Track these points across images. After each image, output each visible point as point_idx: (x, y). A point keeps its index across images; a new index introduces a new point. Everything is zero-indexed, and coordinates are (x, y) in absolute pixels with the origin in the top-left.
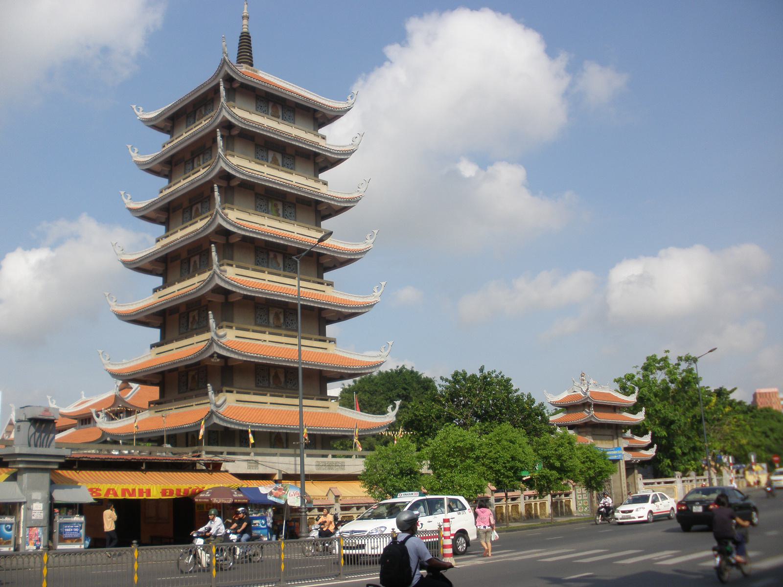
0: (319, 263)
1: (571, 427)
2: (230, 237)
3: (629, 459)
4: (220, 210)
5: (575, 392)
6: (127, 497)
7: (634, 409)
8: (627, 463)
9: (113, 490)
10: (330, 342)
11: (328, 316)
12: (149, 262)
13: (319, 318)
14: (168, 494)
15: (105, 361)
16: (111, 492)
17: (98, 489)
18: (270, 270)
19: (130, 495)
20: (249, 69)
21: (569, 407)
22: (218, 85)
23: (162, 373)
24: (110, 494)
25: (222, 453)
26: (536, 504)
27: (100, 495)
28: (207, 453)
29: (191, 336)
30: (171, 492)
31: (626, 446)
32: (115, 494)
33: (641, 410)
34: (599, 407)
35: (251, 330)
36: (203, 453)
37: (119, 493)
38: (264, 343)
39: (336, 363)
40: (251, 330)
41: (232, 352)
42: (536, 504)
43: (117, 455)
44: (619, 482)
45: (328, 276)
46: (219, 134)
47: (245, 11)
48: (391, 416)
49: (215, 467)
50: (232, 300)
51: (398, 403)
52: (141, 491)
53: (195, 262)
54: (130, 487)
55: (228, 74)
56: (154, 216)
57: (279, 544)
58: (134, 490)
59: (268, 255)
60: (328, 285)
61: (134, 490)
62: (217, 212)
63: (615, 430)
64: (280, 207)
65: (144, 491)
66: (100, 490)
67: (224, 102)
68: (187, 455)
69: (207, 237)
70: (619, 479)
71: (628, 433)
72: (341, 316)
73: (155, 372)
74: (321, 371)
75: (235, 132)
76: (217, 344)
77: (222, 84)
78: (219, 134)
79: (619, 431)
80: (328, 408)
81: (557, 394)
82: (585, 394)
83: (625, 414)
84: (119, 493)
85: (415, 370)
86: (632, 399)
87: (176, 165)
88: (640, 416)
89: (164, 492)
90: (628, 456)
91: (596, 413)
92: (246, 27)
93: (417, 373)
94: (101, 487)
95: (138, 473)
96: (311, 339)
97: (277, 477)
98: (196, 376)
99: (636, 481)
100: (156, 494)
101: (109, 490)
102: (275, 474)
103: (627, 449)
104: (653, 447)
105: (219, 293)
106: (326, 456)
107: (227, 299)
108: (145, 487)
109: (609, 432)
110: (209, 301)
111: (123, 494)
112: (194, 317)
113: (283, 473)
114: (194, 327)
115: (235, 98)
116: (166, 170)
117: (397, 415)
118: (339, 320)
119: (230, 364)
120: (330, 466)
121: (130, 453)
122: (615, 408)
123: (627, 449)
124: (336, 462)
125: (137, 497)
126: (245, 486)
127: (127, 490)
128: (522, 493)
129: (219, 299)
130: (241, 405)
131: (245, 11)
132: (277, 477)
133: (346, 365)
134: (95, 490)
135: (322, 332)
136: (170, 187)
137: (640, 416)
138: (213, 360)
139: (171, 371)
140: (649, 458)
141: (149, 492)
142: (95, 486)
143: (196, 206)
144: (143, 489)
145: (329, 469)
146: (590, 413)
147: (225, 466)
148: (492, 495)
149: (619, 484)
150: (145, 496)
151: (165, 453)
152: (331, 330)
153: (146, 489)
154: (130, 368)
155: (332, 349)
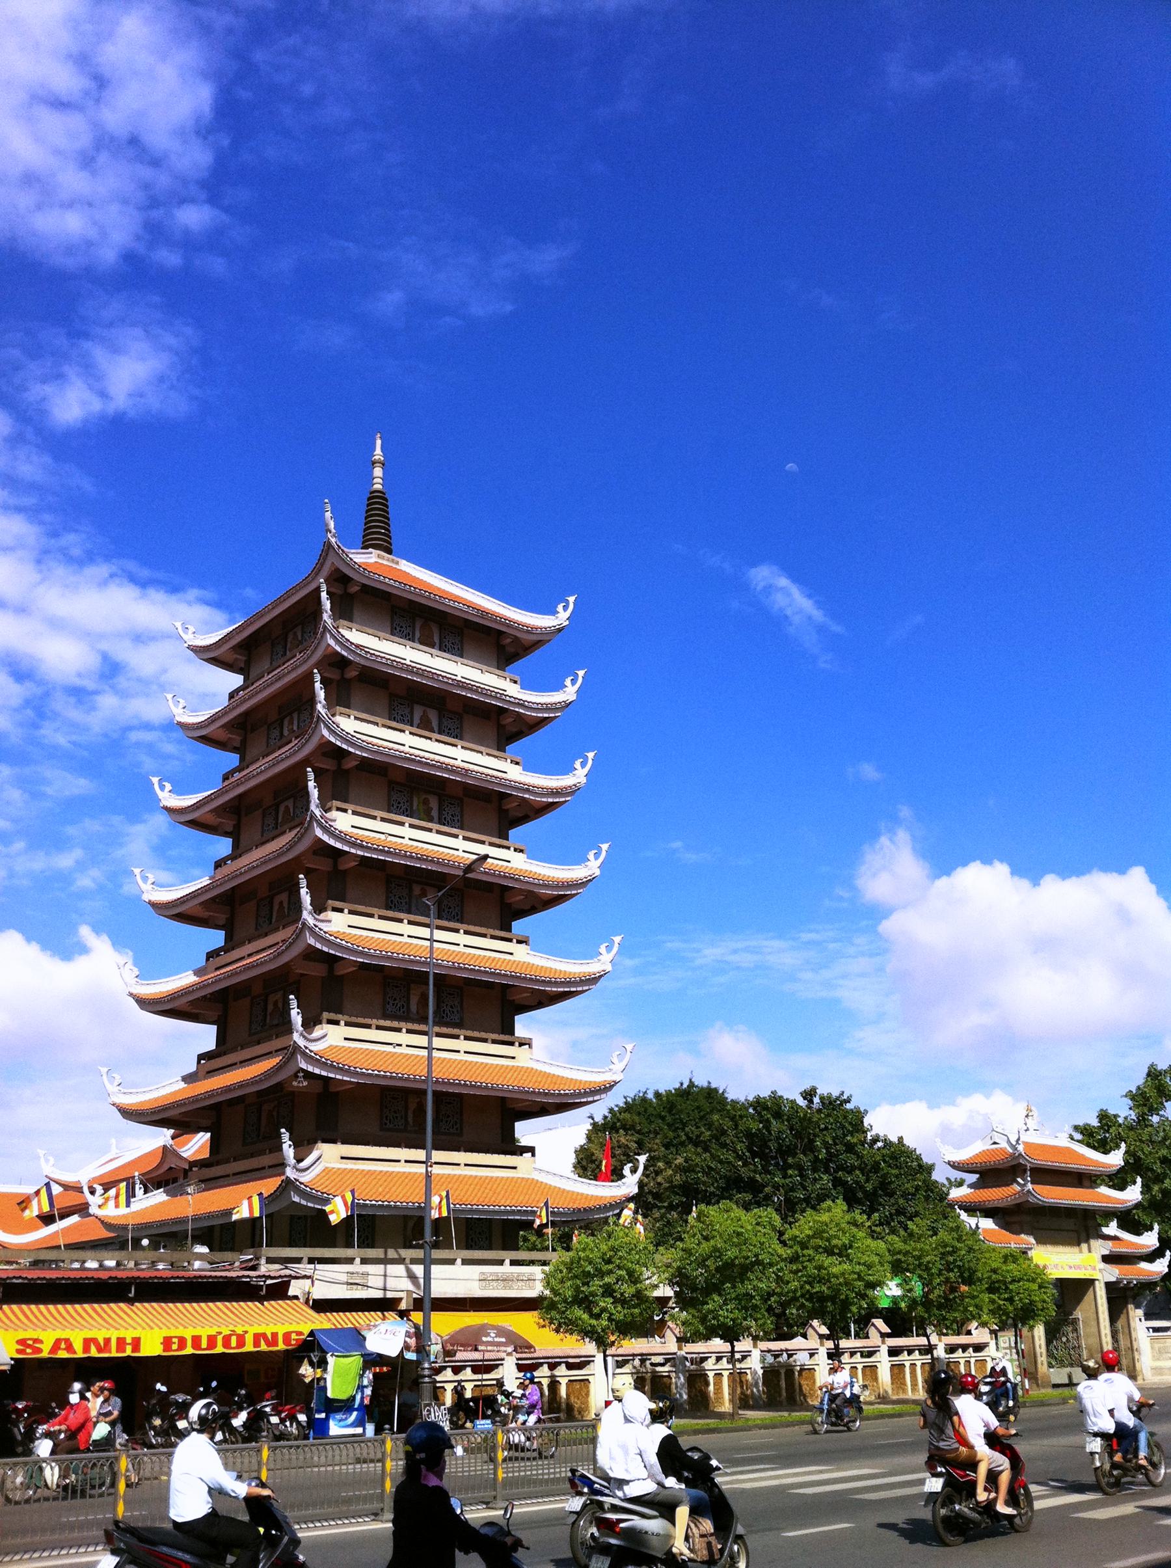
0: (500, 905)
1: (988, 1213)
2: (340, 860)
3: (1114, 1279)
4: (317, 812)
5: (995, 1143)
6: (94, 1353)
7: (1119, 1180)
8: (1108, 1285)
9: (67, 1341)
10: (521, 1045)
11: (517, 998)
12: (200, 904)
13: (493, 1005)
14: (175, 1347)
15: (112, 1088)
16: (63, 1346)
17: (37, 1341)
18: (413, 917)
19: (100, 1350)
20: (383, 558)
21: (994, 1172)
22: (318, 590)
23: (217, 1107)
24: (59, 1348)
25: (298, 1260)
26: (913, 1365)
27: (40, 1351)
28: (270, 1261)
29: (269, 1038)
30: (182, 1342)
31: (1107, 1252)
32: (70, 1347)
33: (1134, 1183)
34: (1044, 1175)
35: (374, 1026)
36: (263, 1261)
37: (78, 1346)
38: (398, 1050)
39: (530, 1084)
40: (374, 1026)
41: (341, 1070)
42: (913, 1365)
43: (96, 1270)
44: (1094, 1323)
45: (519, 926)
46: (318, 678)
47: (378, 451)
48: (629, 1184)
49: (279, 1291)
50: (342, 973)
51: (642, 1159)
52: (121, 1342)
53: (281, 903)
54: (100, 1336)
55: (337, 570)
56: (212, 820)
57: (383, 1442)
58: (107, 1341)
59: (411, 890)
60: (519, 942)
61: (107, 1341)
62: (313, 817)
63: (1079, 1226)
64: (434, 803)
65: (129, 1341)
66: (41, 1342)
67: (329, 621)
68: (233, 1267)
69: (297, 859)
70: (1094, 1318)
71: (1112, 1229)
72: (543, 995)
73: (198, 1106)
74: (503, 1099)
75: (352, 673)
76: (304, 1054)
77: (324, 587)
78: (318, 678)
79: (1090, 1223)
80: (515, 1168)
81: (959, 1146)
82: (1014, 1148)
83: (1104, 1190)
84: (78, 1346)
85: (713, 1086)
86: (1116, 1159)
87: (253, 731)
88: (1133, 1194)
89: (167, 1342)
90: (1112, 1273)
91: (1036, 1187)
92: (380, 481)
93: (716, 1090)
94: (41, 1335)
95: (122, 1305)
96: (485, 1040)
97: (403, 1306)
98: (275, 1114)
99: (1132, 1324)
100: (151, 1348)
101: (58, 1342)
102: (401, 1299)
103: (1107, 1259)
104: (1163, 1256)
105: (318, 961)
106: (501, 1262)
107: (331, 970)
108: (129, 1336)
109: (1069, 1224)
110: (302, 975)
111: (86, 1349)
112: (276, 1003)
113: (415, 1296)
114: (275, 1022)
115: (352, 610)
116: (237, 740)
117: (641, 1185)
118: (540, 1005)
119: (332, 1089)
120: (506, 1280)
121: (118, 1264)
122: (1083, 1178)
123: (1107, 1259)
124: (519, 1274)
125: (114, 1354)
126: (327, 1326)
127: (95, 1341)
128: (883, 1342)
129: (317, 970)
130: (350, 1165)
131: (378, 451)
132: (403, 1306)
133: (546, 1086)
134: (30, 1342)
135: (508, 1028)
136: (243, 769)
137: (1133, 1194)
138: (295, 1083)
139: (231, 1102)
140: (1157, 1278)
141: (136, 1343)
142: (30, 1334)
143: (286, 803)
144: (124, 1339)
145: (505, 1288)
146: (1024, 1185)
147: (295, 1288)
148: (822, 1344)
149: (1095, 1330)
150: (129, 1352)
151: (199, 1261)
152: (523, 1025)
153: (133, 1339)
154: (156, 1100)
155: (523, 1058)
